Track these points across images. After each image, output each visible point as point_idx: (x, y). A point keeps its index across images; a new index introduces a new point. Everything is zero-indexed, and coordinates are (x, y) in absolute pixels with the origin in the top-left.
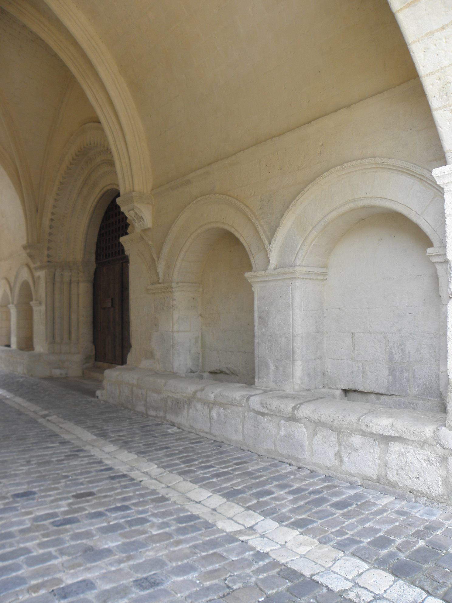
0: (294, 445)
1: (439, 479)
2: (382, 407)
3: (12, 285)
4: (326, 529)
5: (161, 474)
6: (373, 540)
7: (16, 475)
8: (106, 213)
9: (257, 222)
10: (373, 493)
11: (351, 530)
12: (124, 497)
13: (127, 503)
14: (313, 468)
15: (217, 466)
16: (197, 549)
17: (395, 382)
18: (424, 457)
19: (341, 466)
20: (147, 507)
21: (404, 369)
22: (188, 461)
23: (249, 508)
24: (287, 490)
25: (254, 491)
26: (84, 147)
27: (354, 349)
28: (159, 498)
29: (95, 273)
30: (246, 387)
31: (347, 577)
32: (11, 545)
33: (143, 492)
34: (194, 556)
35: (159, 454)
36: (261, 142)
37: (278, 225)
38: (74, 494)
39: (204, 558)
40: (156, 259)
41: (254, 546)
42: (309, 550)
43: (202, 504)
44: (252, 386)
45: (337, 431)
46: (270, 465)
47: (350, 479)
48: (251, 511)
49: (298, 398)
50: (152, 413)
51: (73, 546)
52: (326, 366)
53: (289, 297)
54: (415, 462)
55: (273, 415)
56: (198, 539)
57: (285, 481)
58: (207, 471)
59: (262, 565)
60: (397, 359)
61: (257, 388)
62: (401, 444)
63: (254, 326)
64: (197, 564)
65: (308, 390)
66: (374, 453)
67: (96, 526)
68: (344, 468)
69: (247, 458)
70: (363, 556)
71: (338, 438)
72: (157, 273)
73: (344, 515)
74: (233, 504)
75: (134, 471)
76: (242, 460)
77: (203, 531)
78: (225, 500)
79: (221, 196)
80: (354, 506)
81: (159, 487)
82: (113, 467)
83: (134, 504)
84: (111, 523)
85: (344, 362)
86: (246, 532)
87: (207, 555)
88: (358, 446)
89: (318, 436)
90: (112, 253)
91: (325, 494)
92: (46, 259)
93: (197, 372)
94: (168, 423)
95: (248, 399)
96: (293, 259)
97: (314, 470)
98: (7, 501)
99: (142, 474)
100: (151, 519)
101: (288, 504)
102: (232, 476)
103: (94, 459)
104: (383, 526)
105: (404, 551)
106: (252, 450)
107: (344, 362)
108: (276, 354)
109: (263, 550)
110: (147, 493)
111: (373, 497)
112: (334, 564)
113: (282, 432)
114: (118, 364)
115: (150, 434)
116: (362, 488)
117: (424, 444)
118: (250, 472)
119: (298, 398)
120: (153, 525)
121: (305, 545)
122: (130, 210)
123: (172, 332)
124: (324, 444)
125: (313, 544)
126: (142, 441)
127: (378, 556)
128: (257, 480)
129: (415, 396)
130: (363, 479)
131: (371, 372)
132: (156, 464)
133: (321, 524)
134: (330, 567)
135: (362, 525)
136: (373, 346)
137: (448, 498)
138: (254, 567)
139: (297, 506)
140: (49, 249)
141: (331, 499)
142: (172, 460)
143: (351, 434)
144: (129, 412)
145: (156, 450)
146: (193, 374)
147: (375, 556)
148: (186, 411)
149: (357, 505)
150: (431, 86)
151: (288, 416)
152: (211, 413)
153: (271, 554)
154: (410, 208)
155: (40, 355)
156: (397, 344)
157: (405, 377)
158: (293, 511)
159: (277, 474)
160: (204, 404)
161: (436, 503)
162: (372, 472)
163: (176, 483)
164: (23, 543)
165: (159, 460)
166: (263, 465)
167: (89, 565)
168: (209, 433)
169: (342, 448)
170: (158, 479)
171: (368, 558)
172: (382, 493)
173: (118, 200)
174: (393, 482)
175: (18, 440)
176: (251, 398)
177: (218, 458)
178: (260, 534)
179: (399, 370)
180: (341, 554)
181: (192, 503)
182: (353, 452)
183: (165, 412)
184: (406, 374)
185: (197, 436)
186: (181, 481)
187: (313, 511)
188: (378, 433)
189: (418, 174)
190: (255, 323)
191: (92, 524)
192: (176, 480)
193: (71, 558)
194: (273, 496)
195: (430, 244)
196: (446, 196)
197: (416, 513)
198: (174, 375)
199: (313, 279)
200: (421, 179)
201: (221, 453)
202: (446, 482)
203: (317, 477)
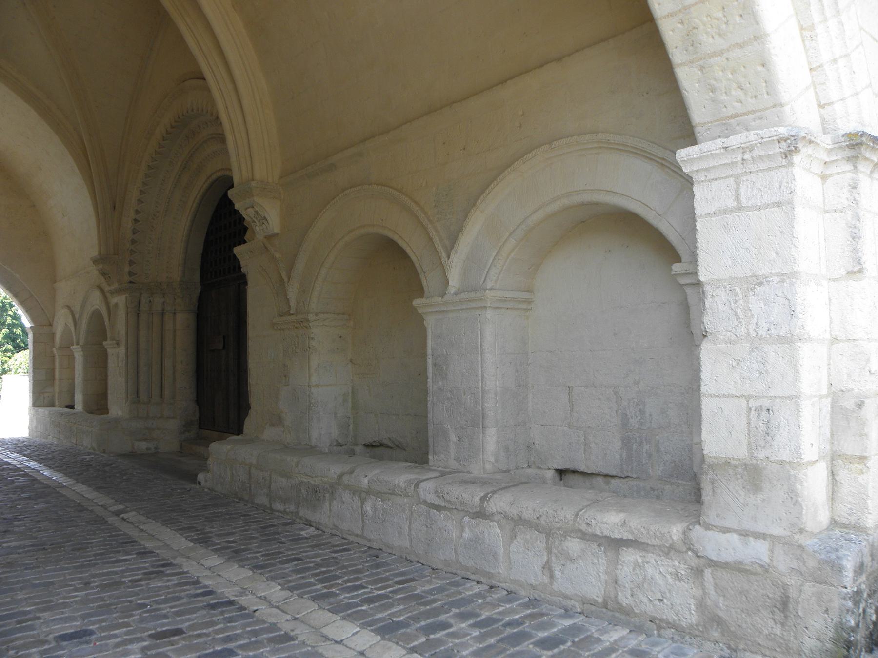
0: (483, 554)
1: (692, 602)
3: (77, 316)
5: (286, 599)
7: (65, 605)
10: (597, 624)
12: (228, 636)
13: (230, 645)
14: (512, 587)
15: (370, 587)
17: (632, 457)
18: (670, 570)
19: (551, 584)
20: (262, 650)
22: (327, 579)
23: (413, 650)
24: (471, 622)
25: (423, 623)
26: (183, 115)
27: (572, 411)
28: (279, 636)
29: (200, 299)
30: (415, 468)
33: (257, 628)
35: (285, 569)
37: (460, 230)
40: (286, 279)
43: (343, 644)
44: (423, 466)
45: (546, 533)
50: (278, 506)
53: (477, 334)
54: (658, 577)
55: (452, 509)
57: (469, 608)
60: (633, 424)
62: (637, 550)
63: (427, 377)
65: (505, 472)
68: (555, 587)
69: (416, 574)
71: (547, 543)
72: (288, 300)
74: (390, 644)
75: (247, 595)
76: (408, 577)
78: (379, 638)
79: (379, 187)
80: (569, 644)
81: (281, 619)
83: (241, 647)
85: (557, 430)
91: (526, 627)
92: (127, 278)
93: (345, 445)
94: (301, 522)
95: (417, 486)
96: (483, 280)
97: (513, 590)
98: (46, 647)
99: (258, 600)
101: (471, 643)
102: (391, 601)
106: (424, 562)
107: (557, 430)
108: (458, 418)
110: (261, 629)
111: (597, 631)
113: (467, 535)
114: (233, 434)
115: (274, 539)
116: (582, 617)
117: (669, 550)
118: (418, 594)
122: (249, 208)
123: (309, 386)
126: (261, 550)
128: (428, 607)
130: (584, 604)
131: (596, 444)
132: (279, 584)
136: (599, 406)
137: (704, 630)
139: (485, 645)
140: (131, 263)
141: (535, 634)
142: (303, 578)
143: (565, 537)
145: (281, 563)
146: (340, 448)
148: (327, 504)
149: (573, 642)
150: (671, 33)
151: (474, 511)
154: (647, 206)
156: (634, 403)
157: (645, 450)
159: (459, 597)
160: (354, 494)
161: (687, 637)
162: (595, 591)
163: (308, 613)
165: (284, 578)
166: (438, 583)
168: (362, 536)
169: (553, 558)
172: (610, 624)
175: (73, 550)
176: (422, 484)
177: (372, 575)
179: (636, 440)
184: (646, 447)
185: (344, 541)
186: (315, 610)
187: (508, 652)
188: (604, 535)
189: (658, 157)
190: (428, 374)
192: (309, 609)
194: (451, 630)
195: (677, 259)
196: (696, 189)
197: (659, 652)
198: (311, 450)
199: (511, 308)
200: (663, 165)
201: (377, 566)
202: (701, 605)
203: (516, 601)
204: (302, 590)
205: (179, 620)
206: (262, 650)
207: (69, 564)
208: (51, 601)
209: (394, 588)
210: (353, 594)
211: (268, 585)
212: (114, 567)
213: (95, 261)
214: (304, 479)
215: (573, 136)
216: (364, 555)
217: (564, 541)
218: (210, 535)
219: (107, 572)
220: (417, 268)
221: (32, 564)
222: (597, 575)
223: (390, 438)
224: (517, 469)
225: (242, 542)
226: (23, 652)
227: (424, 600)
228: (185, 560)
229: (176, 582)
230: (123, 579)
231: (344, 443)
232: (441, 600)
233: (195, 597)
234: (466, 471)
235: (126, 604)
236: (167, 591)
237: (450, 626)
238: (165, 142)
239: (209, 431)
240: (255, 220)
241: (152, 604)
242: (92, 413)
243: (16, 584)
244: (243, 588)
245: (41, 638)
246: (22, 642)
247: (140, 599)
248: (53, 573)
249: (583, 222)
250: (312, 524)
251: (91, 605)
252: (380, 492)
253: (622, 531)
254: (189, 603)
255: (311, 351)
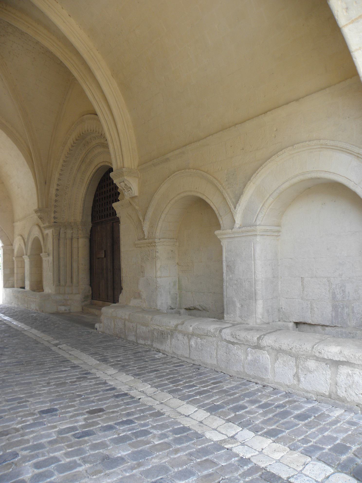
2: (330, 337)
3: (26, 240)
4: (294, 437)
5: (155, 392)
6: (333, 446)
7: (40, 395)
8: (99, 184)
9: (224, 191)
11: (314, 438)
12: (128, 413)
13: (131, 418)
14: (276, 386)
16: (192, 456)
19: (299, 384)
20: (148, 421)
21: (345, 306)
23: (229, 421)
24: (257, 405)
25: (231, 406)
28: (155, 412)
29: (91, 231)
30: (217, 321)
31: (317, 479)
32: (43, 455)
34: (191, 463)
36: (226, 129)
37: (241, 193)
38: (88, 410)
39: (199, 464)
40: (142, 220)
41: (238, 452)
42: (282, 455)
43: (190, 417)
44: (222, 320)
46: (240, 384)
47: (306, 395)
48: (231, 423)
49: (261, 330)
50: (141, 342)
51: (93, 455)
52: (281, 304)
53: (252, 250)
55: (241, 344)
56: (192, 448)
58: (191, 389)
59: (246, 470)
60: (339, 298)
61: (226, 321)
62: (348, 367)
64: (194, 469)
66: (326, 374)
67: (109, 438)
68: (301, 386)
69: (221, 379)
70: (327, 461)
73: (305, 425)
74: (216, 417)
75: (133, 390)
76: (218, 380)
77: (195, 441)
78: (209, 414)
79: (195, 170)
80: (313, 418)
82: (115, 387)
83: (136, 418)
84: (120, 435)
86: (229, 440)
87: (201, 461)
88: (313, 369)
89: (279, 361)
90: (105, 215)
91: (287, 408)
92: (53, 220)
94: (154, 350)
95: (220, 331)
96: (254, 220)
97: (276, 387)
98: (35, 417)
100: (152, 431)
102: (211, 393)
103: (99, 380)
104: (339, 434)
105: (360, 457)
108: (241, 295)
109: (245, 456)
111: (327, 410)
112: (304, 467)
113: (250, 358)
115: (142, 359)
116: (317, 403)
118: (225, 390)
119: (261, 330)
120: (154, 436)
121: (278, 452)
123: (156, 277)
124: (284, 366)
125: (285, 451)
126: (136, 365)
127: (340, 461)
128: (232, 397)
129: (355, 327)
131: (318, 309)
132: (149, 384)
133: (289, 433)
134: (301, 471)
135: (322, 434)
136: (319, 288)
138: (241, 471)
139: (267, 418)
140: (55, 212)
142: (161, 381)
144: (122, 341)
145: (148, 372)
146: (172, 310)
147: (337, 461)
148: (169, 341)
149: (315, 416)
151: (254, 345)
152: (190, 342)
153: (252, 459)
155: (49, 295)
157: (345, 312)
158: (264, 422)
160: (184, 335)
162: (325, 389)
163: (168, 400)
164: (52, 453)
165: (151, 381)
166: (234, 384)
167: (107, 472)
170: (153, 397)
171: (331, 463)
173: (111, 175)
174: (342, 398)
175: (37, 365)
178: (241, 443)
179: (340, 306)
180: (309, 459)
181: (182, 416)
182: (309, 373)
183: (152, 341)
184: (346, 310)
185: (179, 361)
186: (171, 398)
191: (105, 436)
192: (167, 397)
193: (92, 465)
194: (247, 410)
199: (270, 235)
200: (358, 157)
201: (200, 374)
203: (279, 394)
204: (162, 388)
205: (101, 403)
206: (148, 421)
207: (36, 372)
208: (32, 393)
209: (212, 387)
210: (190, 390)
211: (144, 385)
212: (60, 374)
213: (36, 212)
214: (155, 327)
215: (306, 142)
216: (192, 368)
217: (306, 361)
218: (107, 357)
219: (57, 377)
220: (217, 214)
221: (18, 372)
222: (325, 380)
223: (200, 305)
224: (273, 322)
225: (125, 361)
226: (25, 419)
227: (229, 393)
228: (96, 370)
229: (94, 383)
230: (67, 381)
231: (174, 308)
232: (238, 393)
233: (106, 391)
234: (246, 323)
235: (71, 395)
236: (91, 388)
237: (246, 407)
238: (73, 148)
239: (97, 301)
240: (125, 189)
241: (84, 395)
242: (34, 291)
243: (13, 383)
244: (130, 386)
245: (31, 412)
246: (23, 413)
247: (78, 392)
248: (30, 377)
249: (309, 188)
250: (160, 351)
251: (53, 395)
252: (199, 335)
253: (339, 356)
254: (104, 395)
255: (156, 259)
